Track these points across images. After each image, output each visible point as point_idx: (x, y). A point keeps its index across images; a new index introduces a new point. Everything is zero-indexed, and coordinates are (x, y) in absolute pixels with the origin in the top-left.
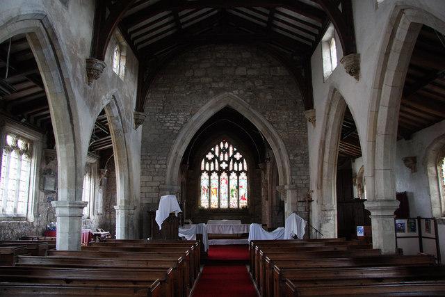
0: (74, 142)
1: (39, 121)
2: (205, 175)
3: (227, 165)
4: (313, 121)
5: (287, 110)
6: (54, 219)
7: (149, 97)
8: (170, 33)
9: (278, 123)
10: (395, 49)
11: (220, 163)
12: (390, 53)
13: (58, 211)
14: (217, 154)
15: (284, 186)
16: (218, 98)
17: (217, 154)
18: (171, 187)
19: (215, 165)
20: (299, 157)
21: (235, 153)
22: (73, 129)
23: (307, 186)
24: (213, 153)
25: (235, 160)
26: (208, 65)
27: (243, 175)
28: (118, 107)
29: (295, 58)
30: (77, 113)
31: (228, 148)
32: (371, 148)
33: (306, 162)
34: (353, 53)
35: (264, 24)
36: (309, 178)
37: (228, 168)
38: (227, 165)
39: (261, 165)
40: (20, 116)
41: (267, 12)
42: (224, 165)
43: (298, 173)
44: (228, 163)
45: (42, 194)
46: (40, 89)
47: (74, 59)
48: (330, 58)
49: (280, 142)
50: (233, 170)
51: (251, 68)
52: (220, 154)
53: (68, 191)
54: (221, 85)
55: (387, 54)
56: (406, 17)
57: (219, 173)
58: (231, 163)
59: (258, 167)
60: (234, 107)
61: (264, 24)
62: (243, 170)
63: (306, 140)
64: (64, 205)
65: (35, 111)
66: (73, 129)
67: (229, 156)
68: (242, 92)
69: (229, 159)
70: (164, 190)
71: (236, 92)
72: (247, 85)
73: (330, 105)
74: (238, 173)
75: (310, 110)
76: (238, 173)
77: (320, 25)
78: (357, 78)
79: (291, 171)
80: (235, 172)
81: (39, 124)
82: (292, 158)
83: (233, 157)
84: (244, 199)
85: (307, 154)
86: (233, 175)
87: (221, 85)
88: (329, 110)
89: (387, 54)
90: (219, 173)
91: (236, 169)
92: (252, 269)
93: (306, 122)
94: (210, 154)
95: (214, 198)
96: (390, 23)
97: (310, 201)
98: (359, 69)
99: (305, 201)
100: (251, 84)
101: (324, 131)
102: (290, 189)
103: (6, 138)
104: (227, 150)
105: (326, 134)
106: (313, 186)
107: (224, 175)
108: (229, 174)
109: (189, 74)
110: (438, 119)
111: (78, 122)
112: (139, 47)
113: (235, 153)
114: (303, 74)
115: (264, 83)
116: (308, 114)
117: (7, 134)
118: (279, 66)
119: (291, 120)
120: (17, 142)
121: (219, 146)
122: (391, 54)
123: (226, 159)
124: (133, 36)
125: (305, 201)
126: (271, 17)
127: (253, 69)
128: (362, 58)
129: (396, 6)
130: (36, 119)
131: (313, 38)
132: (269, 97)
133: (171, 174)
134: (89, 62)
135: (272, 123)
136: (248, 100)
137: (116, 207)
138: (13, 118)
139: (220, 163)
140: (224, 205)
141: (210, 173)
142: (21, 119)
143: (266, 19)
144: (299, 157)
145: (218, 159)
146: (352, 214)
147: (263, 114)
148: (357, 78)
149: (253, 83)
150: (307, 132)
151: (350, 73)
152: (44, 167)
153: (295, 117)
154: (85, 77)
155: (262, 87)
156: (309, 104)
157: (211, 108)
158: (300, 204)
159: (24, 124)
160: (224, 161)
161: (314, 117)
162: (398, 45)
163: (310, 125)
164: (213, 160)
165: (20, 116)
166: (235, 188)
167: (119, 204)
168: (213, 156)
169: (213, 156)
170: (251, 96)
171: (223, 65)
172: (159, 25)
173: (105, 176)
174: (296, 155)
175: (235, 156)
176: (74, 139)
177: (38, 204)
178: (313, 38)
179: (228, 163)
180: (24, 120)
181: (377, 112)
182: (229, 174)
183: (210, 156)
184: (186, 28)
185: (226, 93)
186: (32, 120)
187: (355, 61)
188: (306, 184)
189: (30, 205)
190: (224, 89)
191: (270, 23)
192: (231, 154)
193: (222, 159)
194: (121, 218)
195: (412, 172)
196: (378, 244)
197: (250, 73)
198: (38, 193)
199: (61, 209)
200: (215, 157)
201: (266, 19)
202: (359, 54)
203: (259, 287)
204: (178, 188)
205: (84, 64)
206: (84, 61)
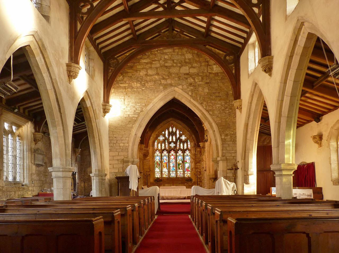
0: (63, 126)
1: (27, 111)
2: (158, 153)
3: (174, 145)
4: (240, 108)
5: (220, 100)
6: (51, 183)
7: (113, 91)
8: (127, 38)
9: (213, 111)
10: (297, 52)
11: (169, 143)
12: (293, 55)
13: (54, 174)
14: (167, 136)
15: (216, 158)
16: (167, 92)
17: (167, 136)
18: (132, 160)
19: (217, 211)
20: (229, 137)
21: (181, 135)
22: (61, 116)
23: (235, 158)
24: (164, 135)
25: (181, 141)
26: (158, 65)
27: (187, 152)
28: (90, 99)
29: (227, 58)
30: (63, 104)
31: (176, 132)
32: (277, 127)
33: (234, 141)
34: (268, 55)
35: (217, 18)
36: (236, 152)
37: (176, 147)
38: (174, 145)
39: (201, 144)
40: (13, 107)
41: (206, 19)
42: (172, 145)
43: (228, 149)
44: (175, 143)
45: (34, 167)
46: (34, 89)
47: (58, 63)
48: (252, 57)
49: (214, 125)
50: (180, 149)
51: (192, 67)
52: (169, 136)
53: (61, 160)
54: (169, 81)
55: (291, 57)
56: (305, 28)
57: (169, 152)
58: (178, 144)
59: (199, 146)
60: (179, 98)
61: (203, 30)
62: (187, 149)
63: (234, 123)
64: (58, 170)
65: (25, 103)
66: (61, 116)
67: (176, 137)
68: (185, 87)
69: (177, 140)
70: (128, 162)
71: (180, 87)
72: (189, 81)
73: (252, 96)
74: (184, 151)
75: (238, 100)
76: (184, 151)
77: (248, 30)
78: (270, 75)
79: (223, 147)
80: (181, 150)
81: (27, 114)
82: (223, 137)
83: (179, 138)
84: (188, 171)
85: (235, 134)
86: (180, 152)
87: (169, 81)
88: (252, 100)
89: (291, 57)
90: (169, 152)
91: (182, 148)
92: (192, 217)
93: (235, 110)
94: (162, 136)
95: (165, 170)
96: (294, 32)
97: (237, 169)
98: (272, 68)
99: (233, 169)
100: (192, 80)
101: (248, 116)
102: (221, 160)
103: (4, 124)
104: (175, 134)
105: (249, 118)
106: (239, 158)
107: (172, 152)
108: (176, 152)
109: (142, 73)
110: (336, 108)
111: (64, 112)
112: (103, 51)
113: (181, 135)
114: (234, 72)
115: (202, 79)
116: (236, 103)
117: (5, 121)
118: (214, 65)
119: (223, 108)
120: (12, 127)
121: (168, 130)
122: (294, 57)
123: (174, 140)
124: (98, 41)
125: (233, 169)
126: (209, 24)
127: (194, 68)
128: (275, 60)
129: (298, 20)
130: (24, 109)
131: (242, 41)
132: (206, 90)
133: (132, 150)
134: (68, 66)
135: (208, 111)
136: (190, 93)
137: (91, 175)
138: (6, 108)
139: (169, 143)
140: (173, 175)
141: (162, 151)
142: (14, 109)
143: (204, 25)
144: (229, 137)
145: (168, 139)
146: (266, 179)
147: (201, 104)
148: (270, 75)
149: (194, 79)
150: (235, 117)
151: (265, 71)
152: (33, 146)
153: (226, 106)
154: (67, 77)
155: (201, 83)
156: (237, 96)
157: (161, 100)
158: (229, 171)
159: (16, 113)
160: (172, 141)
161: (241, 105)
162: (299, 50)
163: (238, 111)
164: (164, 141)
165: (13, 107)
166: (181, 162)
167: (94, 173)
168: (164, 138)
169: (164, 138)
170: (192, 90)
171: (170, 65)
172: (118, 33)
173: (79, 154)
174: (227, 135)
175: (181, 138)
176: (62, 123)
177: (31, 174)
178: (242, 41)
179: (175, 143)
180: (16, 110)
181: (282, 100)
182: (176, 152)
183: (161, 138)
184: (141, 34)
185: (173, 88)
186: (22, 111)
187: (269, 61)
188: (233, 157)
189: (25, 174)
190: (171, 85)
191: (208, 29)
192: (178, 136)
193: (170, 140)
194: (96, 182)
195: (319, 147)
196: (279, 194)
197: (193, 71)
198: (31, 166)
199: (56, 173)
200: (166, 139)
201: (204, 25)
202: (273, 56)
203: (195, 224)
204: (137, 160)
205: (65, 68)
206: (65, 65)
